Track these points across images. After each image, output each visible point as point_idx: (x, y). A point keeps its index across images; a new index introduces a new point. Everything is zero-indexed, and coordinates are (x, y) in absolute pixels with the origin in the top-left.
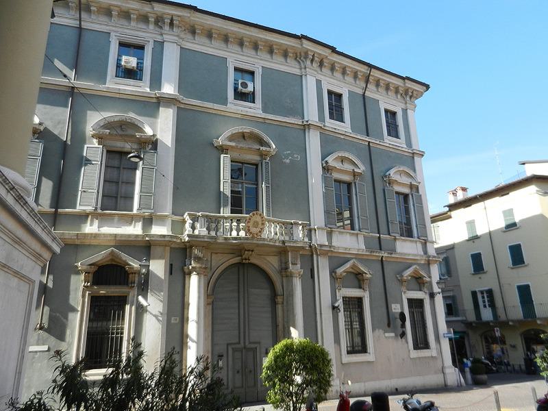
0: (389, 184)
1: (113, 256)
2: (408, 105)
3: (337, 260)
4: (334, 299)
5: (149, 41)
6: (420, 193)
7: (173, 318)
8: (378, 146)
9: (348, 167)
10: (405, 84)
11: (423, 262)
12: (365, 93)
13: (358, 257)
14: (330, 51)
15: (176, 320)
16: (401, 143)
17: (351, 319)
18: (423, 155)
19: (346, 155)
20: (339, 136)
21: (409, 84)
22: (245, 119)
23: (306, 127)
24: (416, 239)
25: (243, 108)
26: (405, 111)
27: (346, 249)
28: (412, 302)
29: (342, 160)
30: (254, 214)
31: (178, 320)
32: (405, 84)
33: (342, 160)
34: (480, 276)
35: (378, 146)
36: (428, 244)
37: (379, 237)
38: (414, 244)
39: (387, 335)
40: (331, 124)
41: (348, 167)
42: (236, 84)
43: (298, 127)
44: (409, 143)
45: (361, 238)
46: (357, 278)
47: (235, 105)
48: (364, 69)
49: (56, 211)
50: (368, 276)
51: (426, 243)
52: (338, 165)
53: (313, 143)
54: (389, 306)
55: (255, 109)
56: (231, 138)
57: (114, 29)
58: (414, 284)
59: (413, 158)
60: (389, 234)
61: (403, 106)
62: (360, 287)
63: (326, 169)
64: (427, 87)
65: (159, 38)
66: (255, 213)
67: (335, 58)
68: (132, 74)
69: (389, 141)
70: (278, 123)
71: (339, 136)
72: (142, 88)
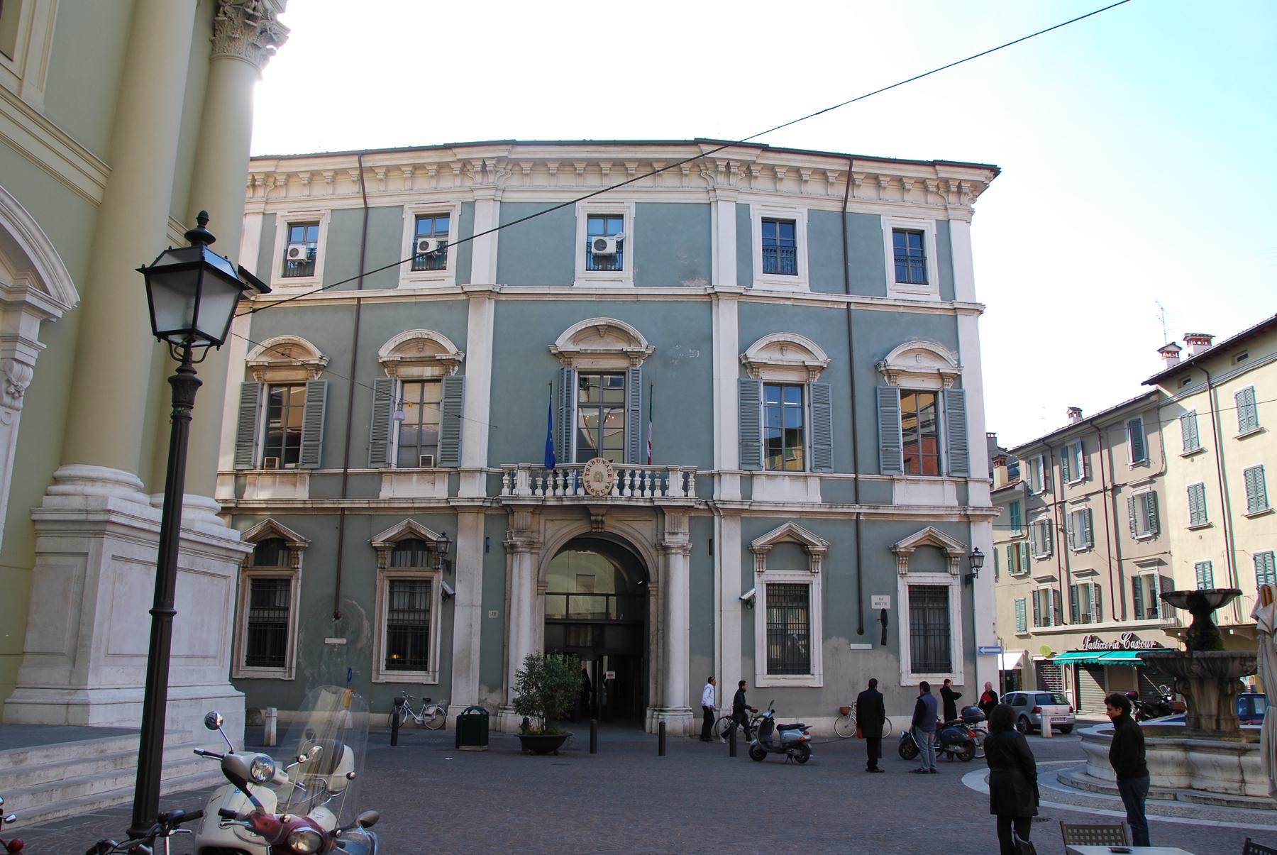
0: (889, 377)
1: (411, 528)
2: (950, 211)
3: (745, 514)
4: (748, 583)
5: (454, 206)
6: (964, 388)
7: (490, 612)
8: (871, 308)
9: (793, 357)
10: (936, 173)
11: (955, 519)
12: (845, 208)
13: (805, 516)
14: (758, 152)
15: (495, 614)
16: (928, 295)
17: (924, 620)
18: (981, 312)
19: (780, 337)
20: (782, 302)
21: (944, 173)
22: (603, 301)
23: (713, 298)
24: (944, 477)
25: (604, 281)
26: (944, 228)
27: (776, 504)
28: (917, 593)
29: (783, 346)
30: (593, 463)
31: (497, 615)
32: (936, 173)
33: (783, 346)
34: (1171, 541)
35: (871, 308)
36: (970, 485)
37: (856, 479)
38: (938, 487)
39: (853, 646)
40: (765, 283)
41: (793, 357)
42: (589, 245)
43: (698, 299)
44: (948, 289)
45: (814, 484)
46: (801, 552)
47: (588, 280)
48: (841, 165)
49: (346, 471)
50: (820, 548)
51: (967, 482)
52: (775, 357)
53: (726, 322)
54: (864, 596)
55: (621, 281)
56: (577, 338)
57: (408, 198)
58: (928, 557)
59: (956, 316)
60: (880, 474)
61: (941, 215)
62: (808, 568)
63: (746, 366)
64: (995, 171)
65: (469, 197)
66: (594, 460)
67: (771, 159)
68: (434, 261)
69: (898, 293)
70: (661, 299)
71: (782, 302)
72: (443, 281)
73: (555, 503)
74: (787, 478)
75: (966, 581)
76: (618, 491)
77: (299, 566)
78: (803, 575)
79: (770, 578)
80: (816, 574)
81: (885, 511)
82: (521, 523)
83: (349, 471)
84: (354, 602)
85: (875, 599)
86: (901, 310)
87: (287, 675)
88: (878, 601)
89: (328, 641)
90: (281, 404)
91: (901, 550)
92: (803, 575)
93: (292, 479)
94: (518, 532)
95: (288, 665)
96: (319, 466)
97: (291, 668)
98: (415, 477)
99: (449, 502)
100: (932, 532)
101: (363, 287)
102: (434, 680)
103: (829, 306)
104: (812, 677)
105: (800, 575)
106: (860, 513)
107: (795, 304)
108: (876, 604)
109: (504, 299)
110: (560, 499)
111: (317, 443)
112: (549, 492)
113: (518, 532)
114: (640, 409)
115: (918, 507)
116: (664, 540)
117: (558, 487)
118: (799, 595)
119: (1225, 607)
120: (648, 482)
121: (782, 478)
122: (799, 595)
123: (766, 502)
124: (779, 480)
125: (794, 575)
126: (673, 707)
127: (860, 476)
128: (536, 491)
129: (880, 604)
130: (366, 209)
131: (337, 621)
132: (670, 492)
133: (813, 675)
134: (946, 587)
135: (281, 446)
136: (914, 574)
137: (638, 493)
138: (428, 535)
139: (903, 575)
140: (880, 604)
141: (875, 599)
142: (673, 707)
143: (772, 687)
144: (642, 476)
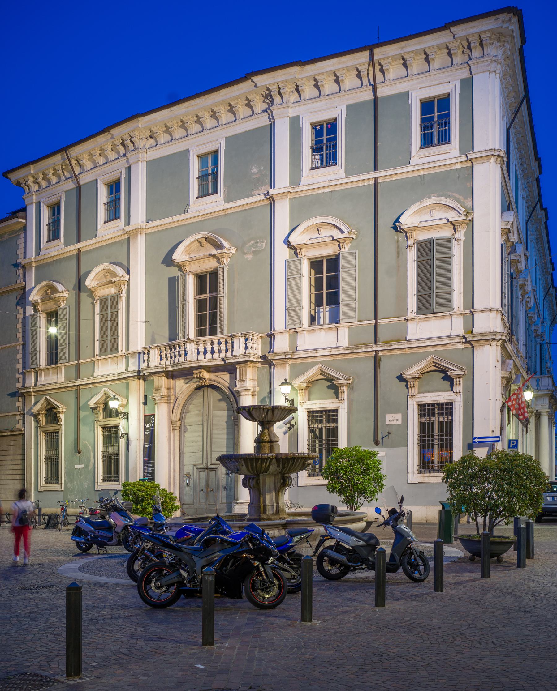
27: (311, 350)
36: (476, 315)
61: (465, 74)
70: (240, 209)
74: (323, 331)
76: (211, 355)
77: (62, 423)
78: (333, 403)
80: (342, 401)
81: (397, 347)
83: (80, 362)
84: (86, 442)
85: (389, 417)
86: (422, 173)
87: (60, 487)
88: (392, 418)
89: (77, 466)
90: (315, 277)
91: (408, 377)
92: (333, 403)
93: (115, 359)
94: (156, 390)
96: (67, 361)
98: (109, 360)
100: (434, 359)
101: (379, 166)
102: (61, 489)
103: (360, 185)
106: (378, 351)
107: (333, 190)
108: (390, 420)
109: (150, 232)
111: (65, 347)
112: (216, 355)
113: (156, 390)
115: (424, 339)
116: (236, 386)
117: (228, 351)
118: (333, 415)
120: (223, 347)
121: (319, 331)
122: (333, 415)
123: (110, 375)
125: (327, 403)
126: (240, 501)
127: (379, 321)
128: (214, 355)
129: (393, 420)
130: (79, 188)
131: (80, 455)
132: (188, 358)
134: (451, 404)
136: (422, 395)
139: (413, 396)
140: (393, 420)
141: (389, 417)
142: (240, 501)
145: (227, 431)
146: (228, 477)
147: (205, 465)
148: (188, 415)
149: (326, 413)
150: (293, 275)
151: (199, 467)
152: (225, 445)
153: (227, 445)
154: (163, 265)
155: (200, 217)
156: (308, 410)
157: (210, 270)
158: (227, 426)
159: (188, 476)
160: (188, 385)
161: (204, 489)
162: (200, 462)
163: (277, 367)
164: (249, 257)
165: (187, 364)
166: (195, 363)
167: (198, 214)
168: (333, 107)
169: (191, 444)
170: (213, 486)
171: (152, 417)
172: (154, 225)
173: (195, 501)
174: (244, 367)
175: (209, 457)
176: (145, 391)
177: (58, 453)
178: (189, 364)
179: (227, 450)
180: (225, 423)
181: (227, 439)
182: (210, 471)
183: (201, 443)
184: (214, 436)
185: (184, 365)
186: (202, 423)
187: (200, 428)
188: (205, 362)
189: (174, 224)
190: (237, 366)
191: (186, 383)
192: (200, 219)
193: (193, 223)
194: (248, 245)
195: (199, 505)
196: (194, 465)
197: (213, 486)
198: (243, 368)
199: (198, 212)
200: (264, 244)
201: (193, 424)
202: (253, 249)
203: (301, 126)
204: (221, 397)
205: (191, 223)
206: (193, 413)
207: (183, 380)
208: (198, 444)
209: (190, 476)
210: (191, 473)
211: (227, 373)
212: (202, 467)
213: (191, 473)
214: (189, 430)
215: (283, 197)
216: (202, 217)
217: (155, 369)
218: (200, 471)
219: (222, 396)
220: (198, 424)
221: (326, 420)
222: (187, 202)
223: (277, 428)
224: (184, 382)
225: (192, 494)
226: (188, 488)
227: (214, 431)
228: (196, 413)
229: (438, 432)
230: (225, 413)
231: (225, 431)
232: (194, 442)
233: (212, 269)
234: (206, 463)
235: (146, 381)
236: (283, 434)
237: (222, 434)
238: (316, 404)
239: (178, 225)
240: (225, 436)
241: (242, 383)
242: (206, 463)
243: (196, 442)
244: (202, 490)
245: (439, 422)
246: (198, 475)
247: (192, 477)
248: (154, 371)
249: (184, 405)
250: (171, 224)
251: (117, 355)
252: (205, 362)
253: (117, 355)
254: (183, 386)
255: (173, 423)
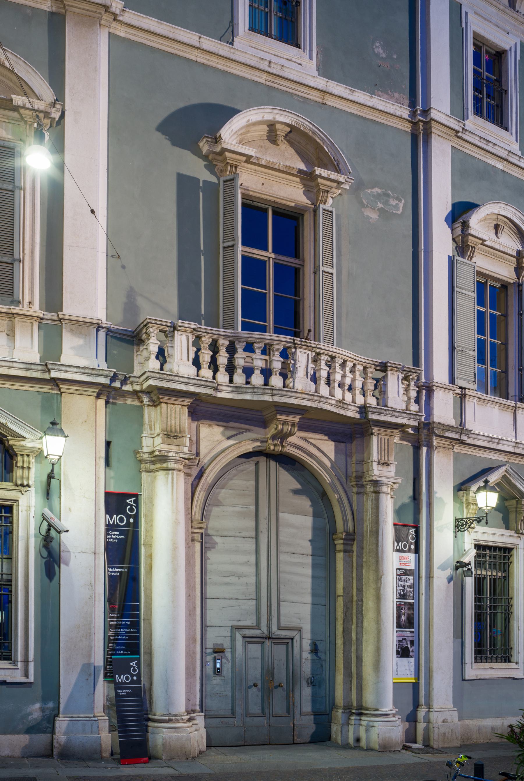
73: (230, 396)
74: (496, 407)
75: (456, 526)
79: (480, 537)
82: (173, 422)
92: (510, 536)
95: (20, 657)
97: (26, 662)
99: (49, 371)
102: (27, 676)
104: (516, 666)
105: (507, 536)
107: (506, 170)
109: (122, 34)
110: (237, 389)
114: (334, 271)
119: (308, 548)
120: (223, 359)
124: (490, 406)
133: (517, 663)
135: (224, 328)
137: (222, 377)
138: (10, 425)
143: (480, 679)
144: (214, 347)
145: (313, 560)
146: (315, 657)
147: (265, 629)
148: (215, 511)
149: (490, 551)
150: (465, 290)
151: (247, 632)
152: (309, 590)
153: (313, 589)
154: (159, 134)
155: (264, 76)
156: (477, 543)
157: (289, 203)
158: (314, 549)
159: (219, 651)
160: (231, 442)
161: (259, 683)
162: (250, 621)
163: (439, 452)
164: (374, 216)
165: (290, 397)
166: (311, 400)
167: (264, 66)
168: (504, 30)
169: (228, 580)
170: (280, 675)
171: (130, 501)
172: (146, 27)
173: (239, 710)
174: (390, 435)
175: (274, 613)
176: (109, 430)
177: (403, 603)
178: (295, 397)
179: (313, 600)
180: (309, 543)
181: (313, 577)
182: (275, 643)
183: (253, 580)
184: (282, 567)
185: (281, 395)
186: (253, 534)
187: (251, 545)
188: (331, 405)
189: (196, 52)
190: (375, 430)
191: (228, 438)
192: (262, 79)
193: (243, 78)
194: (369, 191)
195: (248, 719)
196: (235, 628)
197: (280, 675)
198: (387, 438)
199: (267, 63)
200: (401, 205)
201: (231, 534)
202: (380, 205)
203: (464, 26)
204: (299, 486)
205: (238, 77)
206: (230, 509)
207: (220, 429)
208: (244, 580)
209: (223, 652)
210: (227, 644)
211: (326, 438)
212: (257, 632)
213: (227, 644)
214: (219, 546)
215: (445, 136)
216: (270, 78)
217: (186, 383)
218: (249, 642)
219: (300, 483)
220: (243, 534)
221: (490, 565)
222: (226, 23)
223: (439, 568)
224: (223, 434)
225: (229, 694)
226: (217, 680)
227: (282, 557)
228: (237, 509)
229: (490, 595)
230: (308, 521)
231: (309, 560)
232: (232, 574)
233: (293, 204)
234: (269, 627)
235: (110, 406)
236: (446, 581)
237: (302, 565)
238: (488, 533)
239: (206, 62)
240: (309, 571)
241: (385, 468)
242: (269, 627)
243: (240, 576)
244: (255, 685)
245: (490, 579)
246: (245, 650)
247: (228, 655)
248: (183, 387)
249: (324, 495)
250: (189, 49)
251: (15, 309)
252: (331, 405)
253: (15, 309)
254: (220, 442)
255: (195, 525)
